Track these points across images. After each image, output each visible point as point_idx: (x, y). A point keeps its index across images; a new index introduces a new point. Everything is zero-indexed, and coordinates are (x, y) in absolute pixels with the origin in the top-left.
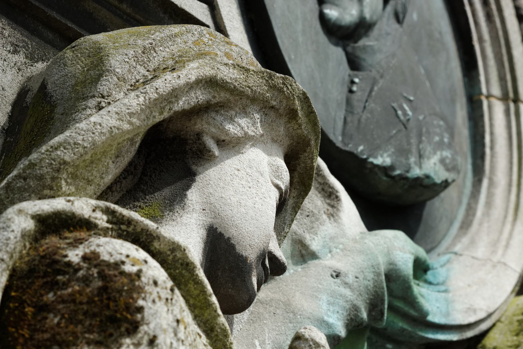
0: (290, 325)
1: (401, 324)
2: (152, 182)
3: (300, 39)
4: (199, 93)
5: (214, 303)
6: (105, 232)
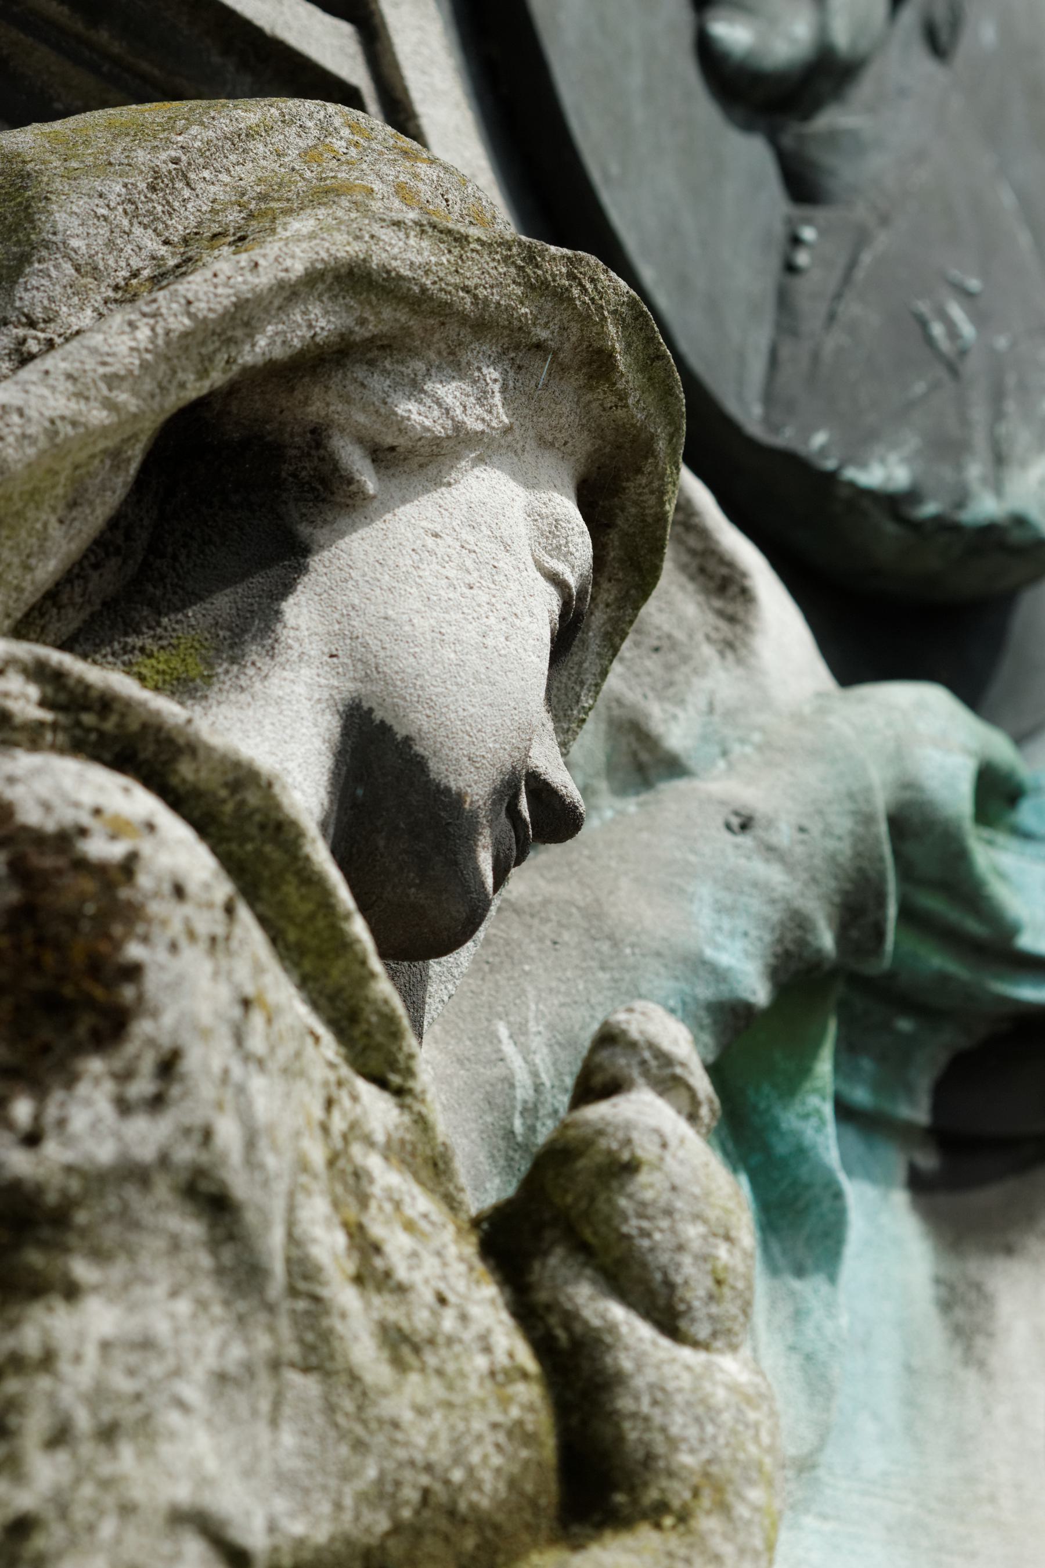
0: (601, 975)
1: (937, 961)
2: (178, 576)
3: (639, 115)
4: (316, 310)
5: (358, 941)
6: (32, 737)
